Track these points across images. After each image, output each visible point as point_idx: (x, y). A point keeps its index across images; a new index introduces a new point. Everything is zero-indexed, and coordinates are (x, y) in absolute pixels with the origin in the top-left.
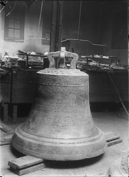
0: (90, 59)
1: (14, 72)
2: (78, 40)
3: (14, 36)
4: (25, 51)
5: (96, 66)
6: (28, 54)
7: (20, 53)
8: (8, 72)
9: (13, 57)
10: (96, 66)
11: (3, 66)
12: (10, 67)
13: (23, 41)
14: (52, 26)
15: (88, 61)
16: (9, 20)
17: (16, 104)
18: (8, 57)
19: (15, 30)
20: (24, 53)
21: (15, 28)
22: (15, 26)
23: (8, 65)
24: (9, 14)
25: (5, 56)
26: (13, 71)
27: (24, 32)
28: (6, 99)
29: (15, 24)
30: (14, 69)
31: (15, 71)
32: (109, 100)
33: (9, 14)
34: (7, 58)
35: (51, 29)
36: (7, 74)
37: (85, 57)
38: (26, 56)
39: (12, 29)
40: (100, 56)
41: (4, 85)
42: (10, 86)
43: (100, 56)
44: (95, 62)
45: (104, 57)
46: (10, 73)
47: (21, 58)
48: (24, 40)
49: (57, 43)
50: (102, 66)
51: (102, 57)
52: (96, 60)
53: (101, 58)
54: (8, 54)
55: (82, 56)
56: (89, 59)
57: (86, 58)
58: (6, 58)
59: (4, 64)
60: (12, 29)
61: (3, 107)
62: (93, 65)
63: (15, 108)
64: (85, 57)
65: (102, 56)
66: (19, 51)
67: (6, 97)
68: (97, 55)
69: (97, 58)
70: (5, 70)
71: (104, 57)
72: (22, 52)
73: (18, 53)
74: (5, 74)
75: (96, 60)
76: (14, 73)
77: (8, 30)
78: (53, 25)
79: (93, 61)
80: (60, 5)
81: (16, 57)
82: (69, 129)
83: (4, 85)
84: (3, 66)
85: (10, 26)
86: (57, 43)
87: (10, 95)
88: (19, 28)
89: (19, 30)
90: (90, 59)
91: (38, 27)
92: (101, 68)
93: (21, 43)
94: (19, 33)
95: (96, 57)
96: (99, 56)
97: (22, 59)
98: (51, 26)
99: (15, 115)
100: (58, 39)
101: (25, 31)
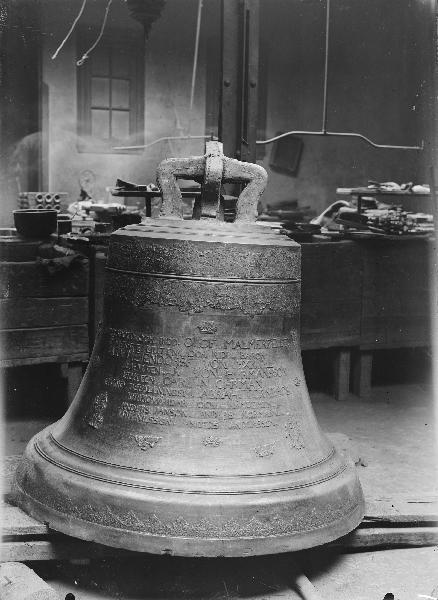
0: (370, 199)
1: (101, 255)
2: (325, 135)
3: (110, 132)
4: (140, 181)
5: (388, 220)
6: (149, 190)
7: (123, 191)
8: (79, 257)
9: (106, 206)
10: (386, 224)
11: (64, 236)
12: (87, 240)
13: (143, 149)
14: (224, 87)
15: (360, 203)
16: (94, 79)
17: (366, 352)
18: (88, 204)
19: (114, 112)
20: (137, 189)
21: (114, 106)
22: (114, 99)
23: (83, 231)
24: (84, 57)
25: (82, 204)
26: (95, 251)
27: (142, 116)
28: (76, 351)
29: (114, 94)
30: (101, 243)
31: (102, 251)
32: (352, 340)
33: (84, 57)
34: (88, 211)
35: (220, 99)
36: (75, 264)
37: (348, 190)
38: (143, 199)
39: (104, 111)
40: (404, 186)
41: (68, 302)
42: (86, 306)
43: (404, 186)
44: (388, 206)
45: (417, 188)
46: (86, 261)
47: (133, 208)
48: (145, 146)
49: (242, 147)
50: (413, 220)
51: (411, 190)
52: (391, 199)
53: (407, 191)
54: (90, 195)
55: (339, 190)
56: (364, 198)
57: (352, 194)
58: (84, 208)
59: (70, 231)
60: (103, 109)
61: (67, 379)
62: (377, 219)
63: (366, 362)
64: (348, 190)
65: (411, 184)
66: (120, 183)
67: (73, 343)
68: (392, 184)
69: (393, 194)
70: (69, 252)
71: (417, 188)
72: (129, 186)
73: (114, 188)
74: (67, 265)
75: (391, 199)
76: (100, 260)
77: (91, 116)
78: (227, 85)
79: (382, 206)
80: (248, 12)
81: (115, 205)
82: (217, 459)
83: (68, 302)
84: (64, 236)
85: (95, 103)
86: (242, 147)
87: (86, 334)
88: (126, 106)
89: (127, 113)
90: (370, 199)
91: (189, 96)
92: (405, 228)
93: (135, 156)
94: (127, 123)
95: (389, 189)
96: (400, 185)
97: (136, 212)
98: (221, 90)
99: (365, 378)
100: (245, 132)
101: (146, 113)
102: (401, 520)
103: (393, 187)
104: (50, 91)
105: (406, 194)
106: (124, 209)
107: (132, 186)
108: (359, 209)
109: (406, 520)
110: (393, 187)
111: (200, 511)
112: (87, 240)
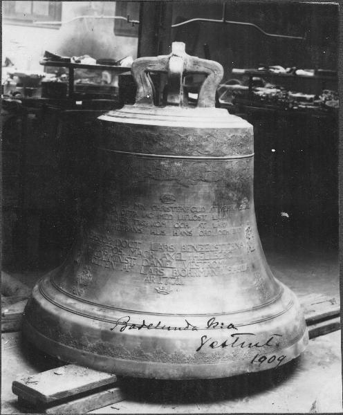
4: (65, 53)
5: (276, 97)
6: (72, 62)
7: (49, 61)
24: (260, 69)
31: (33, 112)
40: (288, 69)
43: (288, 69)
45: (299, 72)
51: (295, 73)
52: (277, 80)
53: (291, 74)
55: (235, 70)
64: (242, 71)
65: (295, 68)
66: (47, 54)
69: (280, 75)
75: (277, 80)
79: (268, 85)
92: (291, 105)
95: (276, 71)
96: (285, 68)
102: (93, 387)
103: (280, 70)
104: (189, 56)
105: (290, 76)
106: (44, 77)
107: (59, 57)
108: (250, 88)
109: (86, 389)
110: (280, 70)
111: (77, 328)
112: (20, 102)
